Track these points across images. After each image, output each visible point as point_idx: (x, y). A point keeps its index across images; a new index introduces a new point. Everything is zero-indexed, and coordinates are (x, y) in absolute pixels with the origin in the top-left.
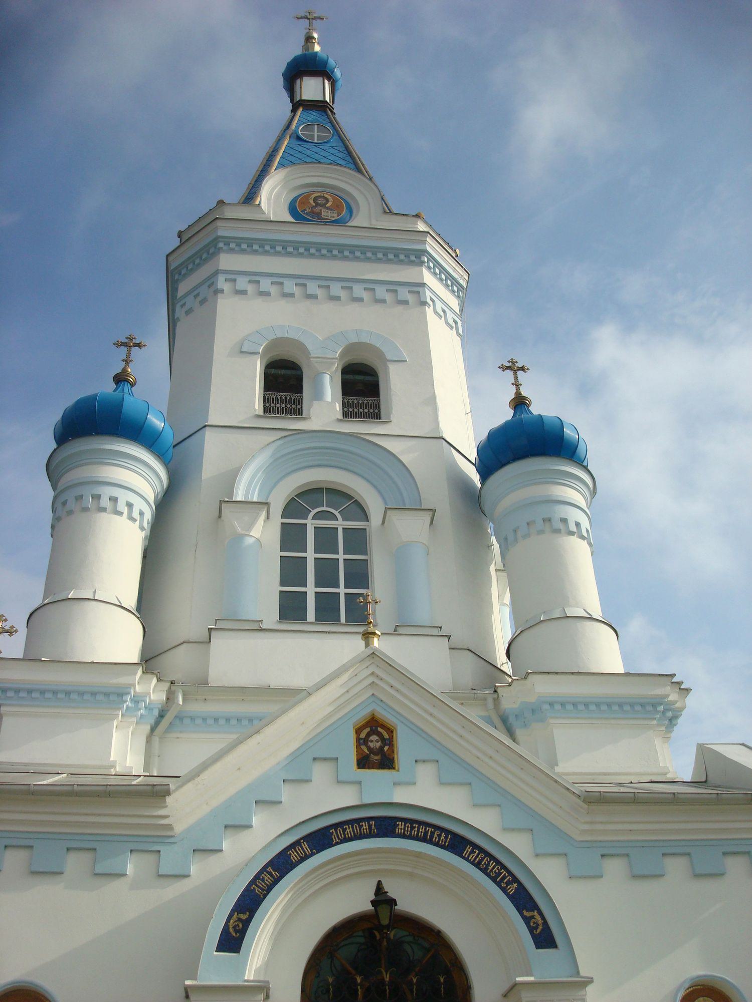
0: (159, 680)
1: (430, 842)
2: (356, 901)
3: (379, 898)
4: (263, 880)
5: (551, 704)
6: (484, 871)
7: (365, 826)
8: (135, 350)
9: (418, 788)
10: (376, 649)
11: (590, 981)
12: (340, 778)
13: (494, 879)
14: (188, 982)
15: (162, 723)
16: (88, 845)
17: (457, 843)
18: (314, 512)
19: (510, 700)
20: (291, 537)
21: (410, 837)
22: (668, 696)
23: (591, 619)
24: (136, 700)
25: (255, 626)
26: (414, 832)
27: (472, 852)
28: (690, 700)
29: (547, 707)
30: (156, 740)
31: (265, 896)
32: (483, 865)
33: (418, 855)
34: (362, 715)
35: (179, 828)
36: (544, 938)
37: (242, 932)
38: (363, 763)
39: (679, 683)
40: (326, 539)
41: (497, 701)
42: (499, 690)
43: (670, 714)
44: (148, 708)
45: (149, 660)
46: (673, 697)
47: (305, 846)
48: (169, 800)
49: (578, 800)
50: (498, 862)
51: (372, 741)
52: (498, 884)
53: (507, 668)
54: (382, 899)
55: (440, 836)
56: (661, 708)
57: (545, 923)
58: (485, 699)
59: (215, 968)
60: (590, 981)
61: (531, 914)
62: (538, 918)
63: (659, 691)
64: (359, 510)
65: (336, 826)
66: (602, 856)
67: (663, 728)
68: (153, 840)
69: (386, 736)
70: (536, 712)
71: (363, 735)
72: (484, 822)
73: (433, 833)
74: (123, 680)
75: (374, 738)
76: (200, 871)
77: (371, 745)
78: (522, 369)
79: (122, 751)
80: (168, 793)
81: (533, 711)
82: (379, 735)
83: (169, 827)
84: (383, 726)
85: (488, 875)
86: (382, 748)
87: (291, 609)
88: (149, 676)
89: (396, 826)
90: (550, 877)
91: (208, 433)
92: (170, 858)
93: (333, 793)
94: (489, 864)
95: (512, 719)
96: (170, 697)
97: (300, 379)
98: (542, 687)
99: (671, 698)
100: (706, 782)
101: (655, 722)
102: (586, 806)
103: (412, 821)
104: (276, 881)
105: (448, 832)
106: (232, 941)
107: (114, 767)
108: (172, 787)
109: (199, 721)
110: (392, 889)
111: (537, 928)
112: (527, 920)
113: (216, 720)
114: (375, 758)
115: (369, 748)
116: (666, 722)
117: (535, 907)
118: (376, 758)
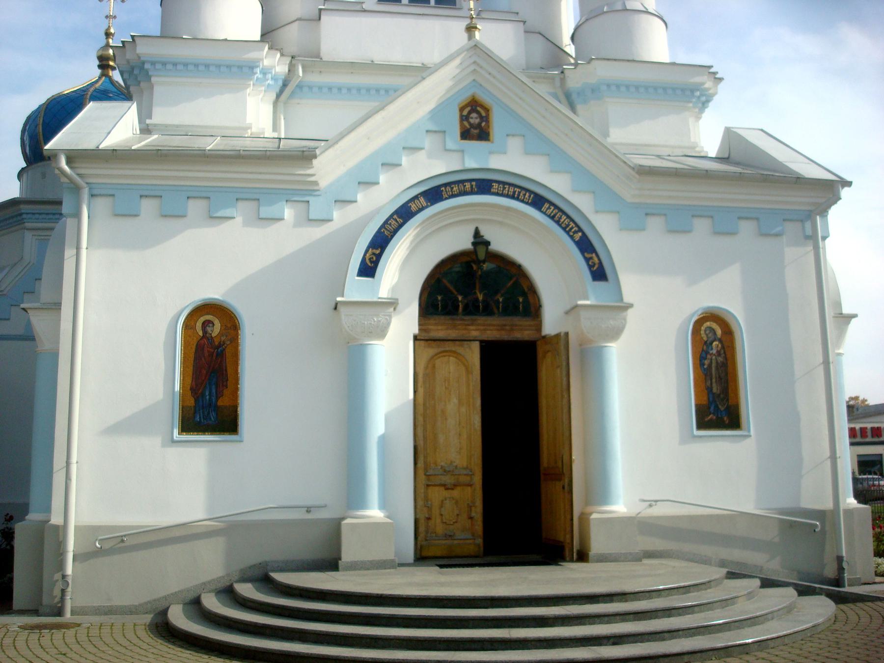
0: (282, 55)
1: (517, 199)
2: (459, 241)
3: (478, 240)
4: (390, 225)
5: (608, 86)
6: (558, 222)
7: (468, 185)
9: (507, 158)
10: (477, 42)
11: (630, 306)
12: (448, 148)
13: (564, 229)
14: (339, 299)
15: (285, 91)
16: (255, 197)
17: (538, 201)
19: (575, 79)
21: (502, 195)
22: (703, 84)
23: (647, 12)
24: (264, 73)
25: (358, 8)
26: (506, 192)
27: (549, 208)
28: (721, 86)
29: (604, 88)
30: (281, 105)
31: (392, 237)
32: (556, 218)
33: (508, 209)
34: (465, 97)
35: (323, 184)
36: (599, 274)
37: (376, 263)
38: (466, 135)
39: (715, 73)
41: (563, 80)
42: (566, 72)
43: (703, 99)
44: (274, 79)
45: (268, 33)
46: (709, 84)
47: (422, 199)
48: (315, 162)
49: (631, 171)
50: (568, 217)
52: (568, 233)
53: (571, 49)
54: (479, 241)
55: (525, 195)
56: (698, 94)
57: (600, 263)
58: (553, 79)
59: (356, 289)
60: (630, 306)
62: (596, 260)
63: (698, 79)
65: (445, 185)
66: (141, 196)
67: (697, 110)
68: (303, 193)
69: (484, 114)
70: (595, 91)
71: (465, 113)
72: (557, 184)
73: (519, 193)
74: (253, 55)
75: (474, 115)
76: (340, 217)
77: (472, 121)
79: (254, 115)
80: (315, 157)
81: (593, 91)
82: (478, 113)
83: (316, 183)
84: (482, 106)
85: (560, 225)
86: (480, 124)
88: (273, 52)
89: (491, 186)
90: (607, 229)
92: (317, 207)
94: (560, 218)
95: (574, 96)
96: (292, 69)
98: (602, 71)
99: (707, 86)
100: (728, 158)
101: (691, 105)
102: (637, 176)
103: (504, 183)
104: (400, 226)
105: (531, 192)
106: (368, 269)
107: (250, 128)
108: (318, 152)
109: (315, 90)
110: (487, 233)
111: (594, 266)
112: (587, 260)
113: (330, 89)
114: (475, 132)
116: (700, 105)
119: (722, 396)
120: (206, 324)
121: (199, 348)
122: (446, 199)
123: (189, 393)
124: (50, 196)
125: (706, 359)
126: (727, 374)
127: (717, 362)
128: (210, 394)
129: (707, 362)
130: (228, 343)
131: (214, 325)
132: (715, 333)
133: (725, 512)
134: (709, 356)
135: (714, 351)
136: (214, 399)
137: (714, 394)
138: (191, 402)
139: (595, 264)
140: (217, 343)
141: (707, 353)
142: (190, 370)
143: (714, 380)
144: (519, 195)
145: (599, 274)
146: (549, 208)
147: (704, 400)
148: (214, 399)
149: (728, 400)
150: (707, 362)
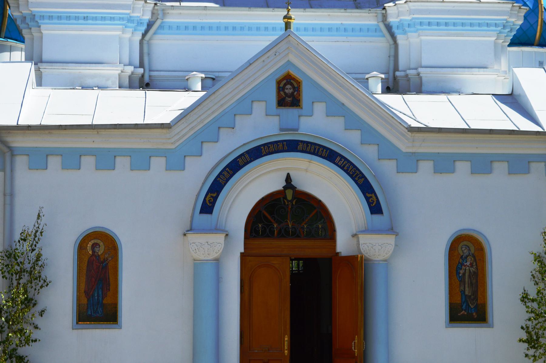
2: (276, 184)
7: (225, 173)
9: (315, 123)
27: (341, 160)
31: (225, 184)
38: (282, 103)
47: (247, 156)
51: (287, 89)
55: (323, 151)
61: (370, 195)
65: (264, 145)
69: (296, 86)
71: (282, 85)
73: (319, 149)
75: (289, 86)
77: (287, 91)
82: (292, 84)
84: (294, 79)
86: (293, 93)
93: (262, 123)
95: (395, 30)
111: (373, 203)
112: (367, 199)
114: (289, 99)
115: (285, 93)
117: (373, 192)
118: (289, 99)
119: (472, 297)
120: (94, 246)
121: (90, 262)
122: (265, 155)
123: (83, 295)
124: (82, 167)
125: (461, 269)
126: (477, 281)
127: (470, 270)
128: (98, 296)
129: (462, 272)
130: (110, 259)
131: (100, 246)
134: (463, 267)
135: (468, 264)
136: (100, 298)
137: (466, 296)
138: (85, 301)
139: (374, 201)
140: (102, 260)
141: (462, 264)
143: (467, 286)
144: (318, 152)
145: (375, 208)
146: (341, 160)
147: (458, 299)
148: (100, 298)
149: (477, 300)
150: (462, 272)
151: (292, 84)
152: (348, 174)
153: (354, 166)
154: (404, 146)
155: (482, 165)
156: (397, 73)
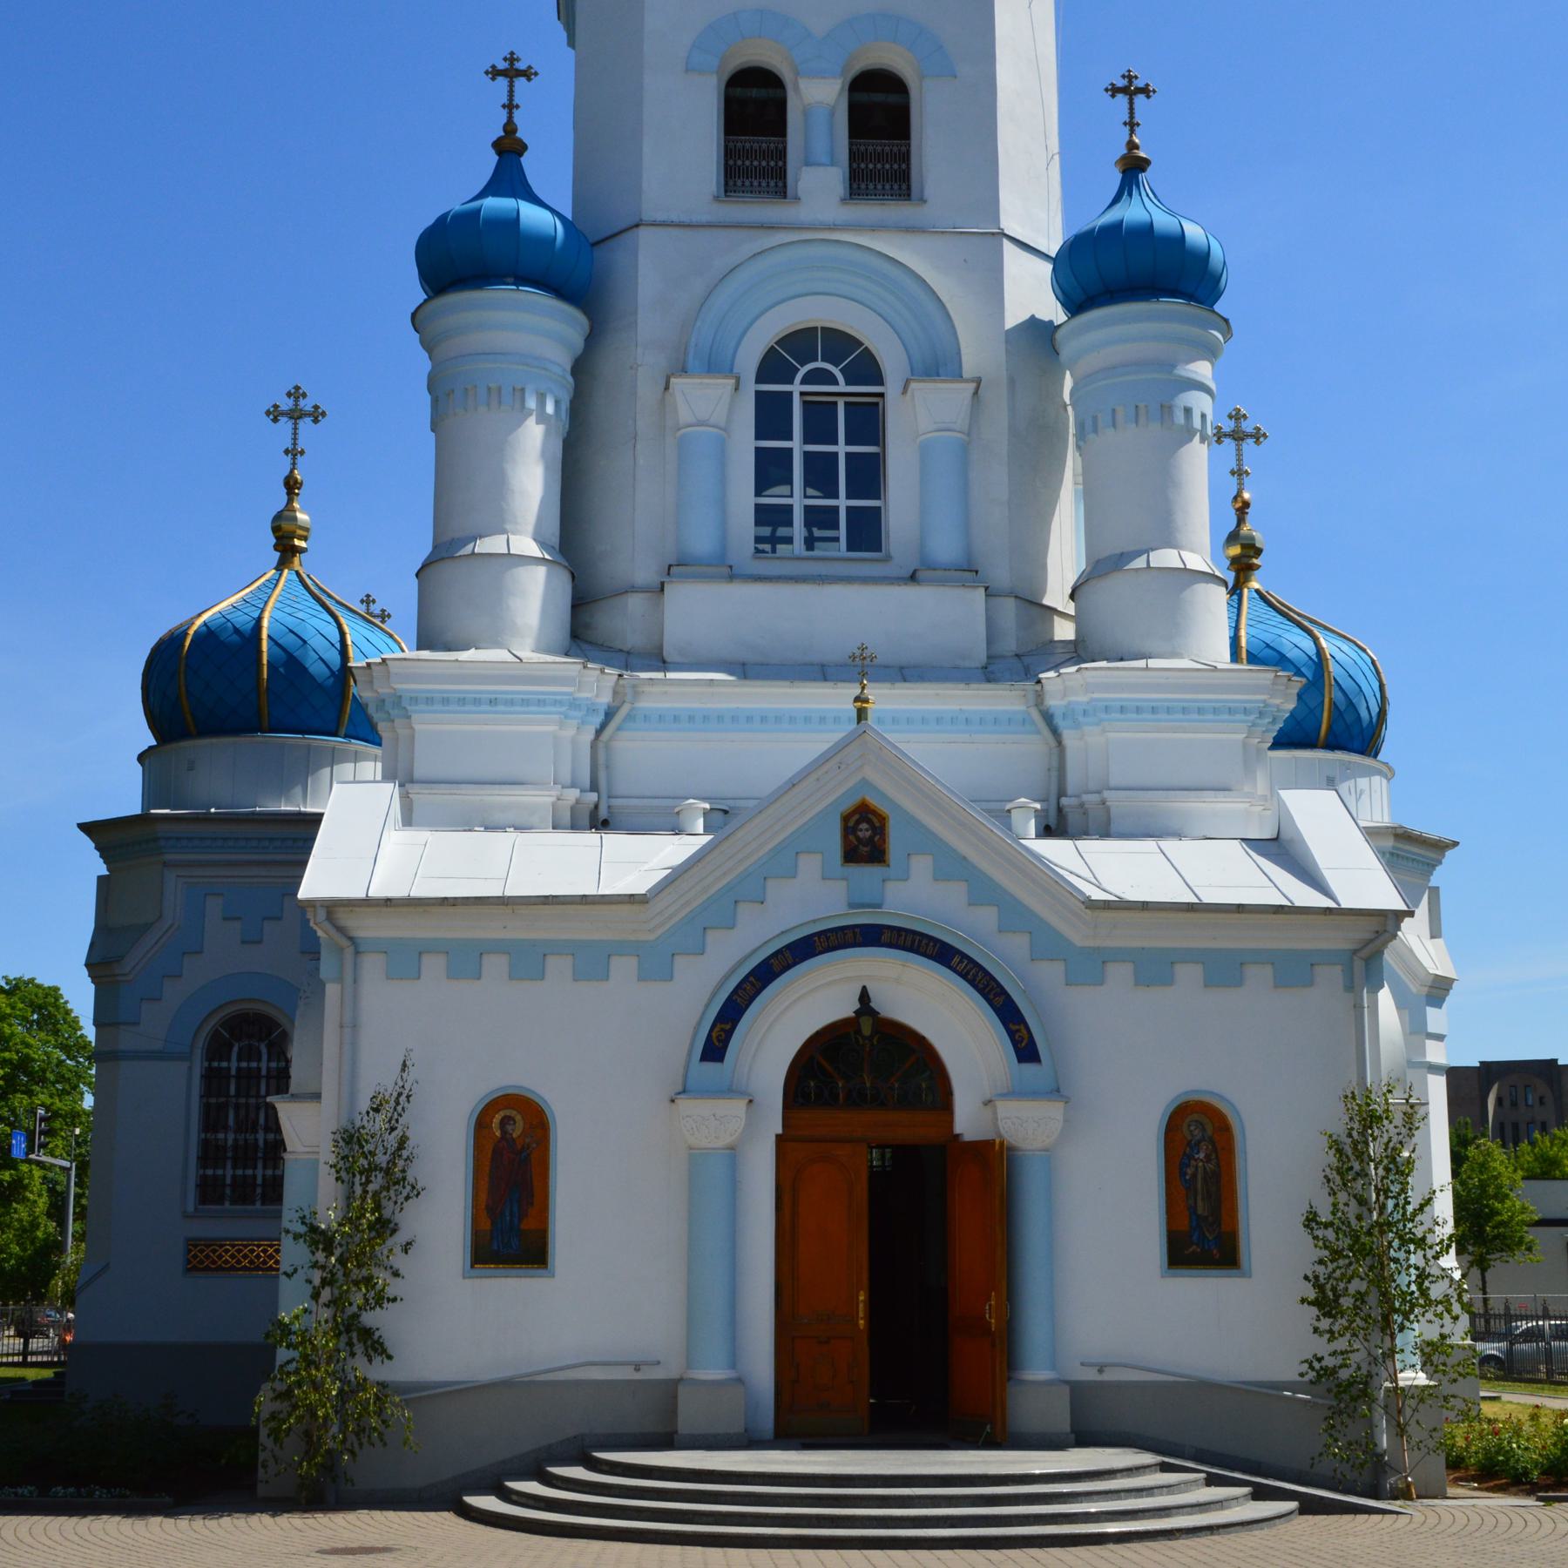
8: (520, 82)
9: (911, 892)
17: (941, 953)
18: (803, 371)
20: (771, 417)
31: (747, 1006)
34: (849, 804)
40: (819, 422)
47: (788, 954)
64: (866, 369)
71: (851, 823)
75: (864, 826)
78: (1145, 91)
82: (869, 821)
84: (874, 812)
86: (871, 838)
87: (771, 518)
91: (644, 234)
93: (817, 893)
95: (1058, 721)
97: (781, 106)
112: (1011, 1034)
114: (864, 850)
115: (858, 838)
120: (505, 1121)
125: (1188, 1166)
132: (1204, 1130)
133: (1171, 1379)
138: (486, 1225)
141: (1191, 1157)
142: (558, 476)
150: (1190, 1171)
151: (869, 821)
152: (975, 986)
153: (987, 973)
154: (1079, 937)
155: (1224, 970)
156: (1064, 801)
